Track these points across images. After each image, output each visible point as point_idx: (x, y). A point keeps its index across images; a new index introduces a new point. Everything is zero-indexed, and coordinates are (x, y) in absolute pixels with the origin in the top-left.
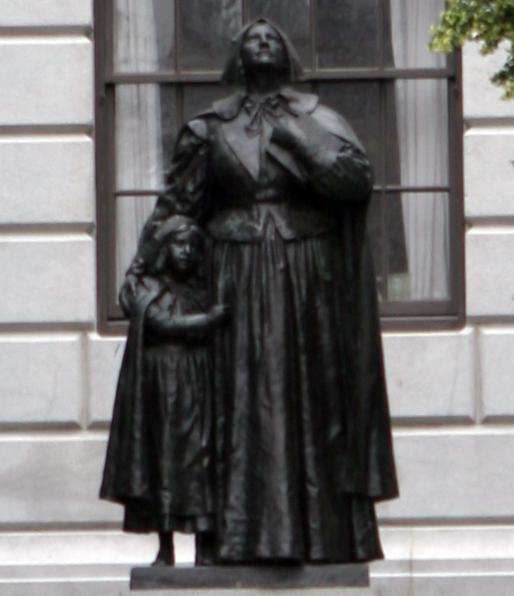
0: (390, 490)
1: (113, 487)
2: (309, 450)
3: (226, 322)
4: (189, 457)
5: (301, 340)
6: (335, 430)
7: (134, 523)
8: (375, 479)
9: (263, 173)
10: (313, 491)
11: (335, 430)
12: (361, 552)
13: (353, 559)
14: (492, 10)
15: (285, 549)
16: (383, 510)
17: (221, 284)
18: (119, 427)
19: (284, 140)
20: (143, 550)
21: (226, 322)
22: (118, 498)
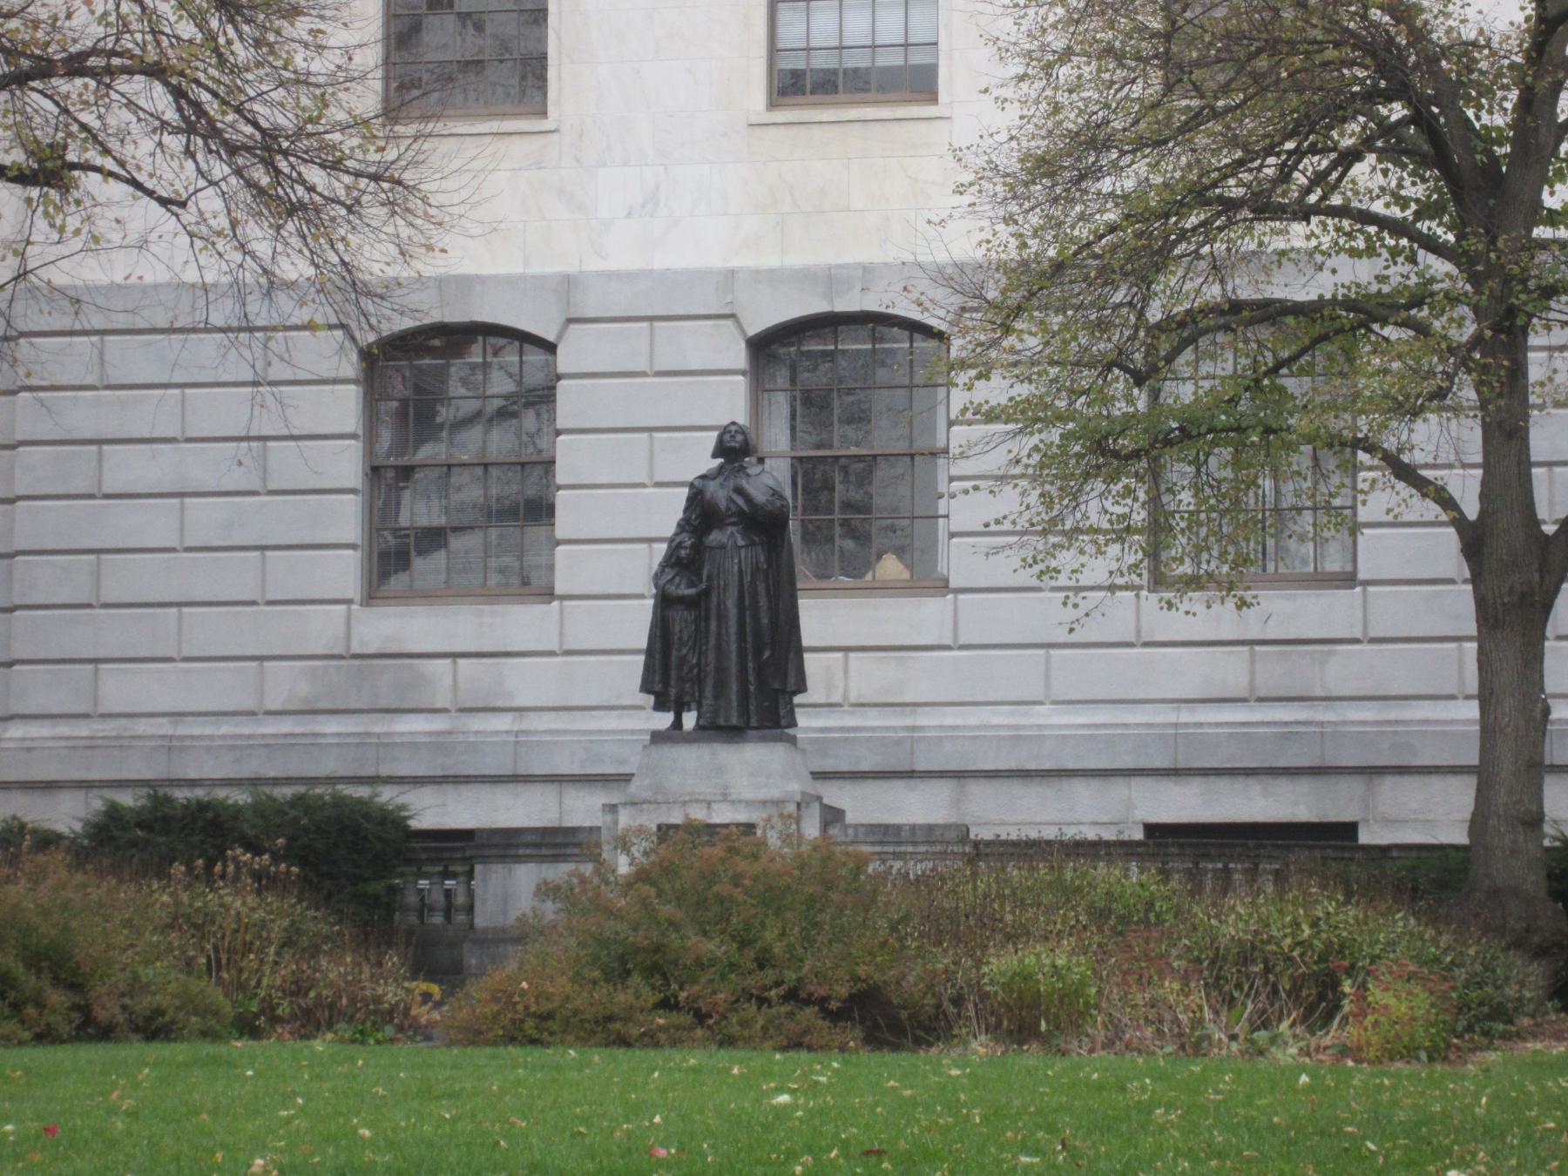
0: (801, 687)
1: (646, 687)
2: (750, 665)
3: (706, 593)
4: (686, 669)
5: (747, 603)
6: (767, 654)
7: (660, 706)
8: (792, 680)
9: (728, 509)
10: (752, 688)
11: (767, 654)
12: (783, 722)
13: (777, 725)
14: (1073, 953)
15: (734, 721)
16: (797, 699)
17: (705, 573)
18: (649, 652)
19: (739, 491)
20: (665, 720)
21: (706, 593)
22: (649, 692)
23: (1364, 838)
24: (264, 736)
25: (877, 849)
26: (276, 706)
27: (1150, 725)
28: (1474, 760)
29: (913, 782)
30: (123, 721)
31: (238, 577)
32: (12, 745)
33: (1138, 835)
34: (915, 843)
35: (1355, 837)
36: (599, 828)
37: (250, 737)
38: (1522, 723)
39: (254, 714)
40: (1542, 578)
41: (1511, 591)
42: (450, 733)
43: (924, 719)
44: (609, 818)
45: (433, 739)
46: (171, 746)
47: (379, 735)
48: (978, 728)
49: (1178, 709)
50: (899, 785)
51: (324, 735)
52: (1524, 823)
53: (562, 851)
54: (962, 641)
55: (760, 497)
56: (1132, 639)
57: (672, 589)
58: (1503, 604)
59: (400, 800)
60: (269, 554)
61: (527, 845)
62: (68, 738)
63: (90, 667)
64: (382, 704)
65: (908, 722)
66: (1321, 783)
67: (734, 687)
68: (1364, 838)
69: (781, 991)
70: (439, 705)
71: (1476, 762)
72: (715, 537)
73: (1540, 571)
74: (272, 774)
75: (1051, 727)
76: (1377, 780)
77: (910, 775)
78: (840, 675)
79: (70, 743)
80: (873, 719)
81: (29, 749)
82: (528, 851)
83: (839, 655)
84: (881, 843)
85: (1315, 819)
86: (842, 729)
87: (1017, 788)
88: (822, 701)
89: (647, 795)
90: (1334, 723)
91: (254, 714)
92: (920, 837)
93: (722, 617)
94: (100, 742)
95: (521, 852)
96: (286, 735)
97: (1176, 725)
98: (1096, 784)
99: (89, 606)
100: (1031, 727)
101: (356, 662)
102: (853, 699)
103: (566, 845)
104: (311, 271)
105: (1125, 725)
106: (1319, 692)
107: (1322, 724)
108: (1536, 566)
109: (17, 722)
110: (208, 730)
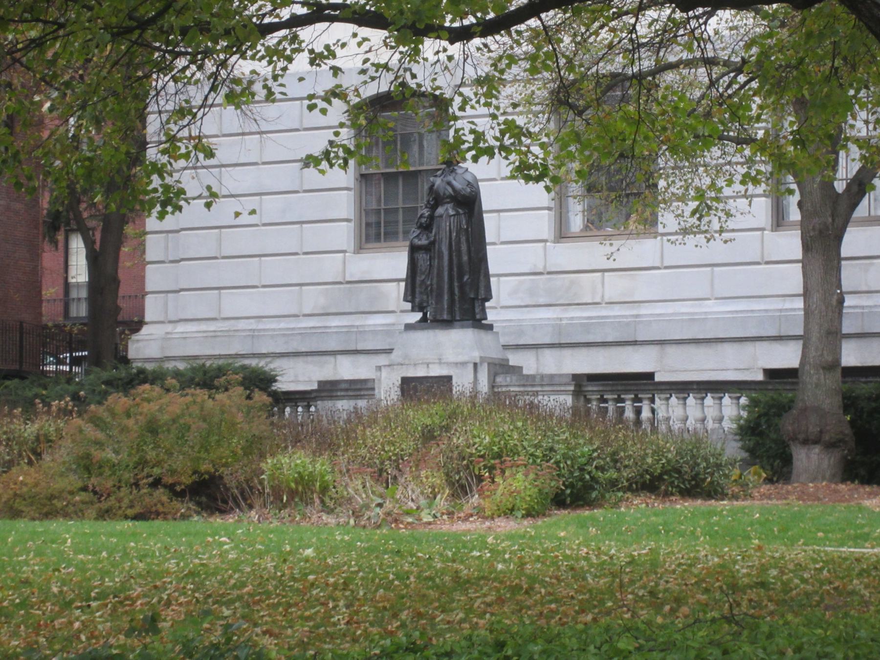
2: (456, 284)
3: (433, 243)
6: (466, 278)
10: (456, 298)
15: (445, 317)
16: (487, 304)
19: (449, 183)
23: (657, 378)
24: (300, 328)
25: (522, 389)
26: (307, 311)
27: (766, 311)
28: (800, 332)
29: (636, 347)
30: (232, 322)
31: (287, 239)
32: (177, 336)
33: (760, 377)
34: (542, 385)
35: (653, 379)
36: (374, 380)
37: (293, 329)
38: (823, 308)
39: (297, 316)
40: (833, 220)
41: (814, 229)
42: (394, 324)
43: (645, 310)
44: (378, 374)
45: (385, 328)
46: (253, 335)
47: (357, 327)
48: (672, 314)
49: (784, 300)
50: (630, 349)
51: (330, 327)
52: (824, 368)
53: (358, 393)
54: (666, 264)
55: (458, 185)
56: (759, 260)
57: (417, 242)
58: (810, 237)
59: (272, 366)
60: (304, 226)
61: (341, 390)
62: (204, 332)
63: (216, 292)
64: (362, 309)
65: (635, 312)
66: (863, 342)
67: (446, 297)
68: (657, 378)
69: (151, 480)
70: (390, 309)
71: (802, 333)
72: (440, 210)
73: (833, 216)
74: (304, 350)
75: (710, 313)
76: (540, 351)
77: (635, 343)
78: (600, 286)
79: (205, 335)
80: (617, 311)
81: (185, 338)
82: (342, 393)
83: (599, 274)
84: (524, 386)
85: (859, 365)
86: (598, 317)
87: (692, 349)
88: (590, 301)
89: (400, 360)
90: (870, 307)
91: (297, 316)
92: (546, 381)
93: (441, 257)
94: (219, 334)
95: (339, 394)
96: (311, 328)
97: (781, 310)
98: (736, 346)
99: (216, 258)
100: (701, 313)
101: (348, 286)
102: (607, 299)
103: (360, 390)
104: (621, 55)
105: (510, 321)
106: (864, 288)
107: (863, 307)
108: (829, 213)
109: (182, 323)
110: (273, 326)
